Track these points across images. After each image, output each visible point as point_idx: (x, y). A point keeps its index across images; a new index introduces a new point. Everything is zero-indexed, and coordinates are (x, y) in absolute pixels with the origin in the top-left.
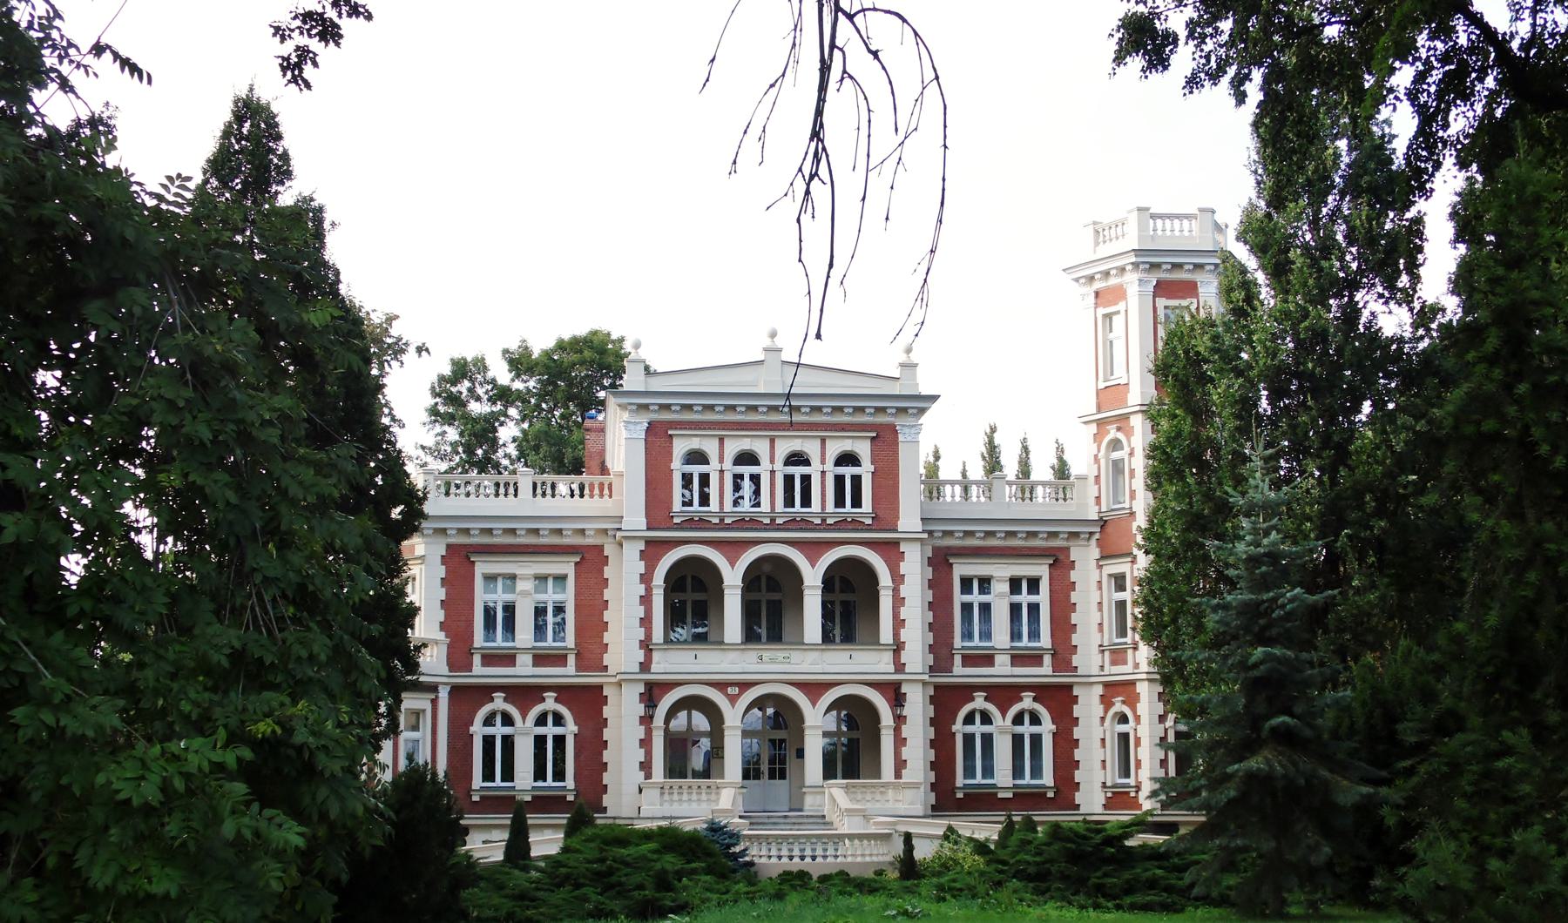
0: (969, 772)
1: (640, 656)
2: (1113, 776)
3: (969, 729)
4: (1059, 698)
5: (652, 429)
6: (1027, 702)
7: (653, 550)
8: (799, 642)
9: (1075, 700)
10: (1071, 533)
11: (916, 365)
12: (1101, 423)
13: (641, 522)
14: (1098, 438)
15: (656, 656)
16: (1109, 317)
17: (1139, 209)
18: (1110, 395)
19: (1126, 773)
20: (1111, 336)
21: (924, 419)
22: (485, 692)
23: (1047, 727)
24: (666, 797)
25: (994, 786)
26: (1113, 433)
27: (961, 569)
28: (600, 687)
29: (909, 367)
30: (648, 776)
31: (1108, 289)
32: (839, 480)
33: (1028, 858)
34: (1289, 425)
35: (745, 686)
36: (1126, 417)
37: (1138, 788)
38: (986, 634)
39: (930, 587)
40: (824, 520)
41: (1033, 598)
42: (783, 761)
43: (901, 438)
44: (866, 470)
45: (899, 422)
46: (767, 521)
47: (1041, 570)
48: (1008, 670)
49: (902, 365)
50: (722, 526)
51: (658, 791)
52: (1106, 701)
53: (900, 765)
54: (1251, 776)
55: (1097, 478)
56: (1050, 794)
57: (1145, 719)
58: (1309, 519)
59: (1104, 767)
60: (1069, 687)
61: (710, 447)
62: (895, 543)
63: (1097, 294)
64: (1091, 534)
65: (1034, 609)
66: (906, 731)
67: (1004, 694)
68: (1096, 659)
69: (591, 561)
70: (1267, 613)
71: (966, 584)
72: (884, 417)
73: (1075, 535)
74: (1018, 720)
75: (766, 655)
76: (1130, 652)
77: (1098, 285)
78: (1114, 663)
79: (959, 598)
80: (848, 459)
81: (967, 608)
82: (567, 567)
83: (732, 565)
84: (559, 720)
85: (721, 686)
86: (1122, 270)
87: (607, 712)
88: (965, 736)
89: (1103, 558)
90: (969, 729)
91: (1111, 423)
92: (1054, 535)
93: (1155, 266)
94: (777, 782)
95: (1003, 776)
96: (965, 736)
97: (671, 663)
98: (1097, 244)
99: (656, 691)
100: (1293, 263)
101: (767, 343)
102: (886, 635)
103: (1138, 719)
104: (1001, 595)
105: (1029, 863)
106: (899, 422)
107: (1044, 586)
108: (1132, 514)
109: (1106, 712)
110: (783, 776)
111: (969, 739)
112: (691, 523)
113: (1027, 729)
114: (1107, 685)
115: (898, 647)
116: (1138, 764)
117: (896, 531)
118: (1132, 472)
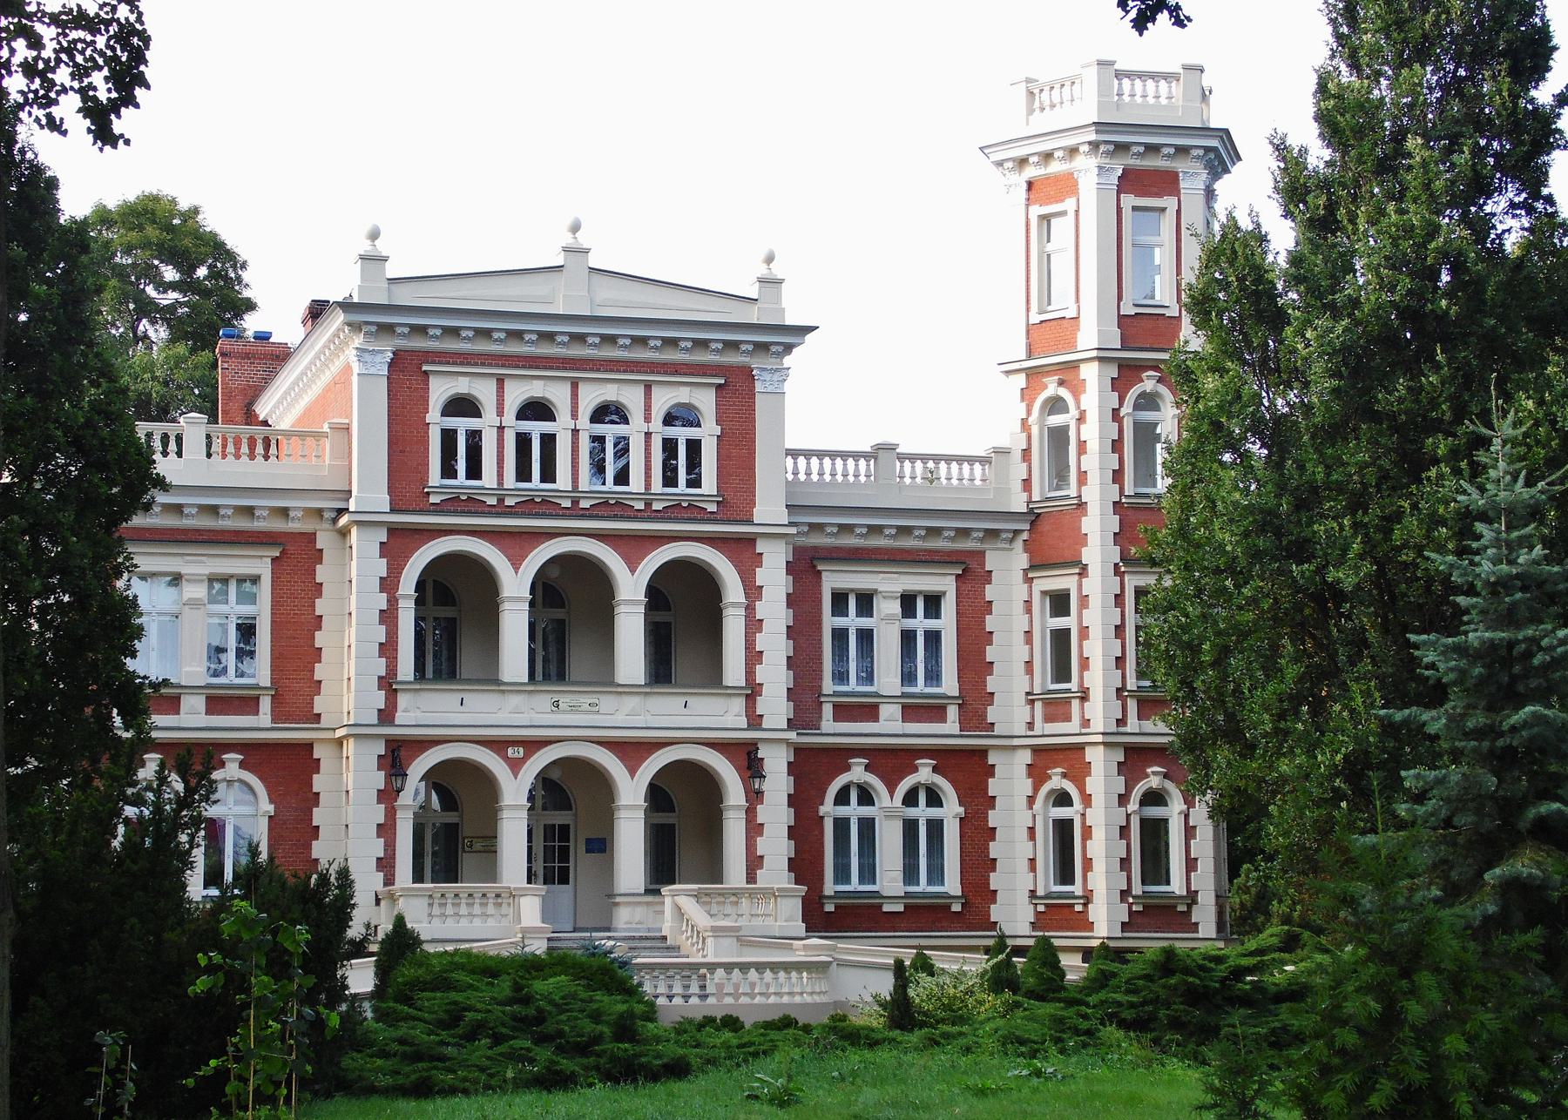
0: (842, 874)
1: (379, 700)
2: (1046, 882)
3: (842, 811)
4: (969, 768)
5: (399, 362)
6: (925, 773)
7: (399, 541)
8: (490, 679)
9: (990, 771)
10: (958, 530)
11: (781, 282)
12: (1031, 373)
13: (381, 500)
14: (1027, 395)
15: (403, 700)
16: (1046, 219)
17: (1100, 63)
18: (1048, 333)
19: (1065, 875)
20: (1049, 247)
21: (788, 361)
22: (839, 757)
23: (951, 810)
24: (436, 910)
25: (876, 894)
26: (1052, 388)
27: (834, 579)
28: (308, 746)
29: (771, 283)
30: (389, 881)
31: (1047, 178)
32: (523, 441)
33: (1118, 997)
34: (1409, 388)
35: (533, 745)
36: (1073, 366)
37: (1087, 899)
38: (868, 676)
39: (789, 605)
40: (648, 504)
41: (932, 624)
42: (564, 854)
43: (759, 387)
44: (708, 433)
45: (756, 363)
46: (567, 504)
47: (944, 583)
48: (898, 726)
49: (761, 281)
50: (501, 510)
51: (425, 901)
52: (1037, 773)
53: (754, 863)
54: (1512, 886)
55: (1026, 454)
56: (957, 908)
57: (1098, 800)
58: (1443, 523)
59: (1033, 868)
60: (982, 752)
61: (484, 392)
62: (751, 540)
63: (1030, 185)
64: (1016, 532)
65: (933, 638)
66: (762, 814)
67: (892, 761)
68: (1021, 713)
69: (296, 559)
70: (1528, 655)
71: (840, 599)
72: (736, 357)
73: (992, 534)
74: (910, 799)
75: (565, 701)
76: (1075, 704)
77: (1031, 172)
78: (1048, 719)
79: (829, 622)
80: (678, 416)
81: (840, 635)
82: (260, 564)
83: (516, 567)
84: (934, 799)
85: (498, 745)
86: (1073, 151)
87: (319, 783)
88: (836, 820)
89: (1033, 567)
90: (842, 811)
91: (1049, 374)
92: (964, 533)
93: (1122, 148)
94: (557, 887)
95: (890, 881)
96: (836, 820)
97: (423, 710)
98: (1030, 111)
99: (403, 753)
100: (1410, 155)
101: (568, 240)
102: (734, 670)
103: (1087, 800)
104: (889, 618)
105: (1119, 1004)
106: (756, 363)
107: (949, 607)
108: (1081, 506)
109: (1036, 789)
110: (564, 880)
111: (842, 825)
112: (455, 504)
113: (922, 812)
114: (1036, 750)
115: (752, 692)
116: (1088, 864)
117: (750, 522)
118: (1082, 447)
